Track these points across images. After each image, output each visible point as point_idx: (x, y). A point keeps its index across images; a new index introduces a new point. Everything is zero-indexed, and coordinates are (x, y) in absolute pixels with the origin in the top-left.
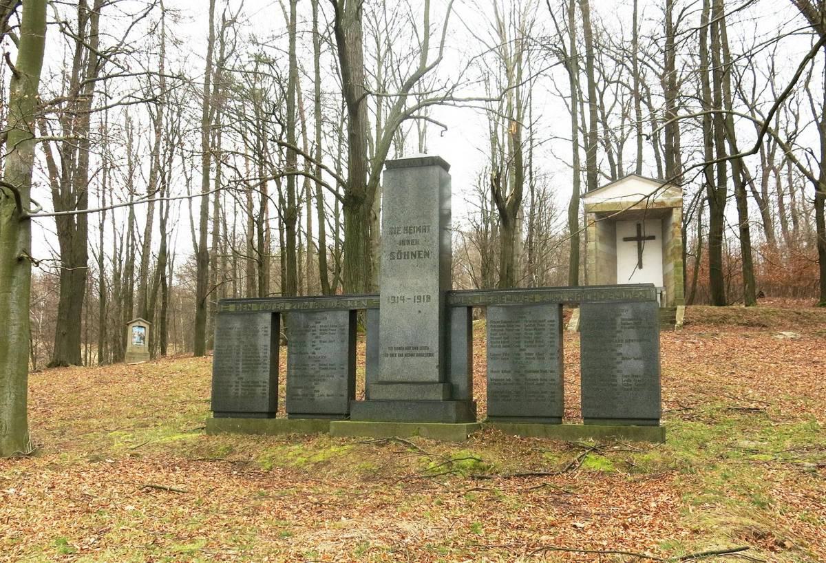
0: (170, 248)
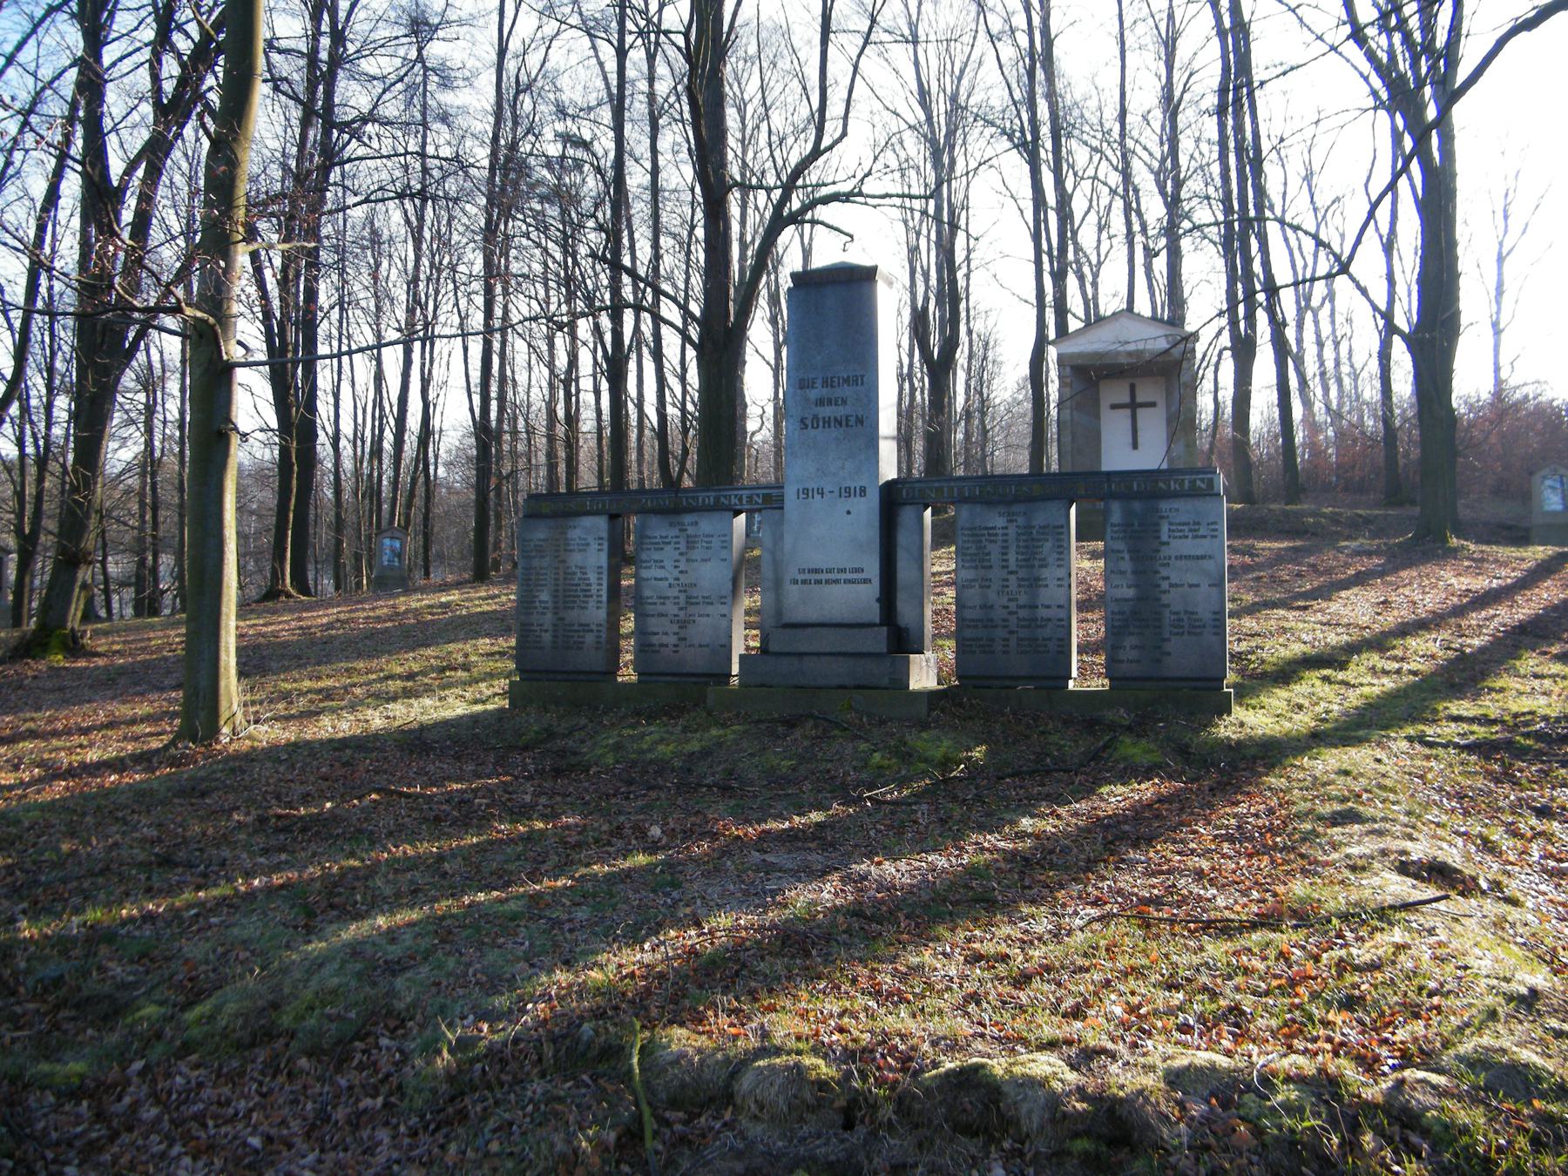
0: (436, 423)
